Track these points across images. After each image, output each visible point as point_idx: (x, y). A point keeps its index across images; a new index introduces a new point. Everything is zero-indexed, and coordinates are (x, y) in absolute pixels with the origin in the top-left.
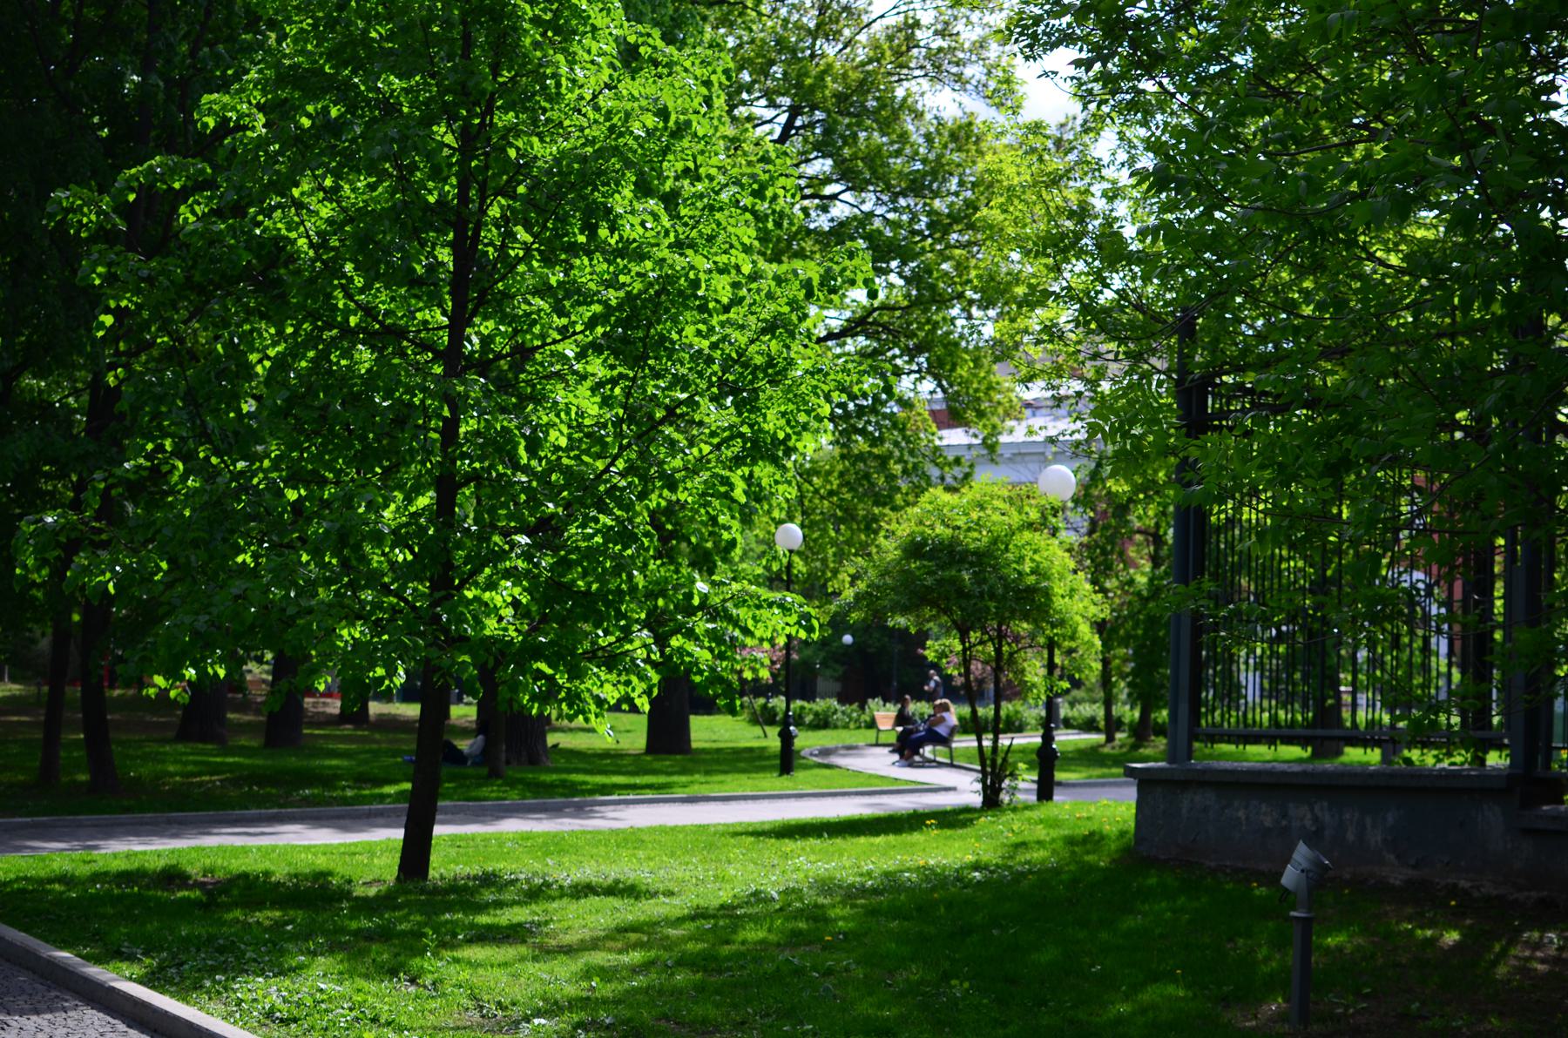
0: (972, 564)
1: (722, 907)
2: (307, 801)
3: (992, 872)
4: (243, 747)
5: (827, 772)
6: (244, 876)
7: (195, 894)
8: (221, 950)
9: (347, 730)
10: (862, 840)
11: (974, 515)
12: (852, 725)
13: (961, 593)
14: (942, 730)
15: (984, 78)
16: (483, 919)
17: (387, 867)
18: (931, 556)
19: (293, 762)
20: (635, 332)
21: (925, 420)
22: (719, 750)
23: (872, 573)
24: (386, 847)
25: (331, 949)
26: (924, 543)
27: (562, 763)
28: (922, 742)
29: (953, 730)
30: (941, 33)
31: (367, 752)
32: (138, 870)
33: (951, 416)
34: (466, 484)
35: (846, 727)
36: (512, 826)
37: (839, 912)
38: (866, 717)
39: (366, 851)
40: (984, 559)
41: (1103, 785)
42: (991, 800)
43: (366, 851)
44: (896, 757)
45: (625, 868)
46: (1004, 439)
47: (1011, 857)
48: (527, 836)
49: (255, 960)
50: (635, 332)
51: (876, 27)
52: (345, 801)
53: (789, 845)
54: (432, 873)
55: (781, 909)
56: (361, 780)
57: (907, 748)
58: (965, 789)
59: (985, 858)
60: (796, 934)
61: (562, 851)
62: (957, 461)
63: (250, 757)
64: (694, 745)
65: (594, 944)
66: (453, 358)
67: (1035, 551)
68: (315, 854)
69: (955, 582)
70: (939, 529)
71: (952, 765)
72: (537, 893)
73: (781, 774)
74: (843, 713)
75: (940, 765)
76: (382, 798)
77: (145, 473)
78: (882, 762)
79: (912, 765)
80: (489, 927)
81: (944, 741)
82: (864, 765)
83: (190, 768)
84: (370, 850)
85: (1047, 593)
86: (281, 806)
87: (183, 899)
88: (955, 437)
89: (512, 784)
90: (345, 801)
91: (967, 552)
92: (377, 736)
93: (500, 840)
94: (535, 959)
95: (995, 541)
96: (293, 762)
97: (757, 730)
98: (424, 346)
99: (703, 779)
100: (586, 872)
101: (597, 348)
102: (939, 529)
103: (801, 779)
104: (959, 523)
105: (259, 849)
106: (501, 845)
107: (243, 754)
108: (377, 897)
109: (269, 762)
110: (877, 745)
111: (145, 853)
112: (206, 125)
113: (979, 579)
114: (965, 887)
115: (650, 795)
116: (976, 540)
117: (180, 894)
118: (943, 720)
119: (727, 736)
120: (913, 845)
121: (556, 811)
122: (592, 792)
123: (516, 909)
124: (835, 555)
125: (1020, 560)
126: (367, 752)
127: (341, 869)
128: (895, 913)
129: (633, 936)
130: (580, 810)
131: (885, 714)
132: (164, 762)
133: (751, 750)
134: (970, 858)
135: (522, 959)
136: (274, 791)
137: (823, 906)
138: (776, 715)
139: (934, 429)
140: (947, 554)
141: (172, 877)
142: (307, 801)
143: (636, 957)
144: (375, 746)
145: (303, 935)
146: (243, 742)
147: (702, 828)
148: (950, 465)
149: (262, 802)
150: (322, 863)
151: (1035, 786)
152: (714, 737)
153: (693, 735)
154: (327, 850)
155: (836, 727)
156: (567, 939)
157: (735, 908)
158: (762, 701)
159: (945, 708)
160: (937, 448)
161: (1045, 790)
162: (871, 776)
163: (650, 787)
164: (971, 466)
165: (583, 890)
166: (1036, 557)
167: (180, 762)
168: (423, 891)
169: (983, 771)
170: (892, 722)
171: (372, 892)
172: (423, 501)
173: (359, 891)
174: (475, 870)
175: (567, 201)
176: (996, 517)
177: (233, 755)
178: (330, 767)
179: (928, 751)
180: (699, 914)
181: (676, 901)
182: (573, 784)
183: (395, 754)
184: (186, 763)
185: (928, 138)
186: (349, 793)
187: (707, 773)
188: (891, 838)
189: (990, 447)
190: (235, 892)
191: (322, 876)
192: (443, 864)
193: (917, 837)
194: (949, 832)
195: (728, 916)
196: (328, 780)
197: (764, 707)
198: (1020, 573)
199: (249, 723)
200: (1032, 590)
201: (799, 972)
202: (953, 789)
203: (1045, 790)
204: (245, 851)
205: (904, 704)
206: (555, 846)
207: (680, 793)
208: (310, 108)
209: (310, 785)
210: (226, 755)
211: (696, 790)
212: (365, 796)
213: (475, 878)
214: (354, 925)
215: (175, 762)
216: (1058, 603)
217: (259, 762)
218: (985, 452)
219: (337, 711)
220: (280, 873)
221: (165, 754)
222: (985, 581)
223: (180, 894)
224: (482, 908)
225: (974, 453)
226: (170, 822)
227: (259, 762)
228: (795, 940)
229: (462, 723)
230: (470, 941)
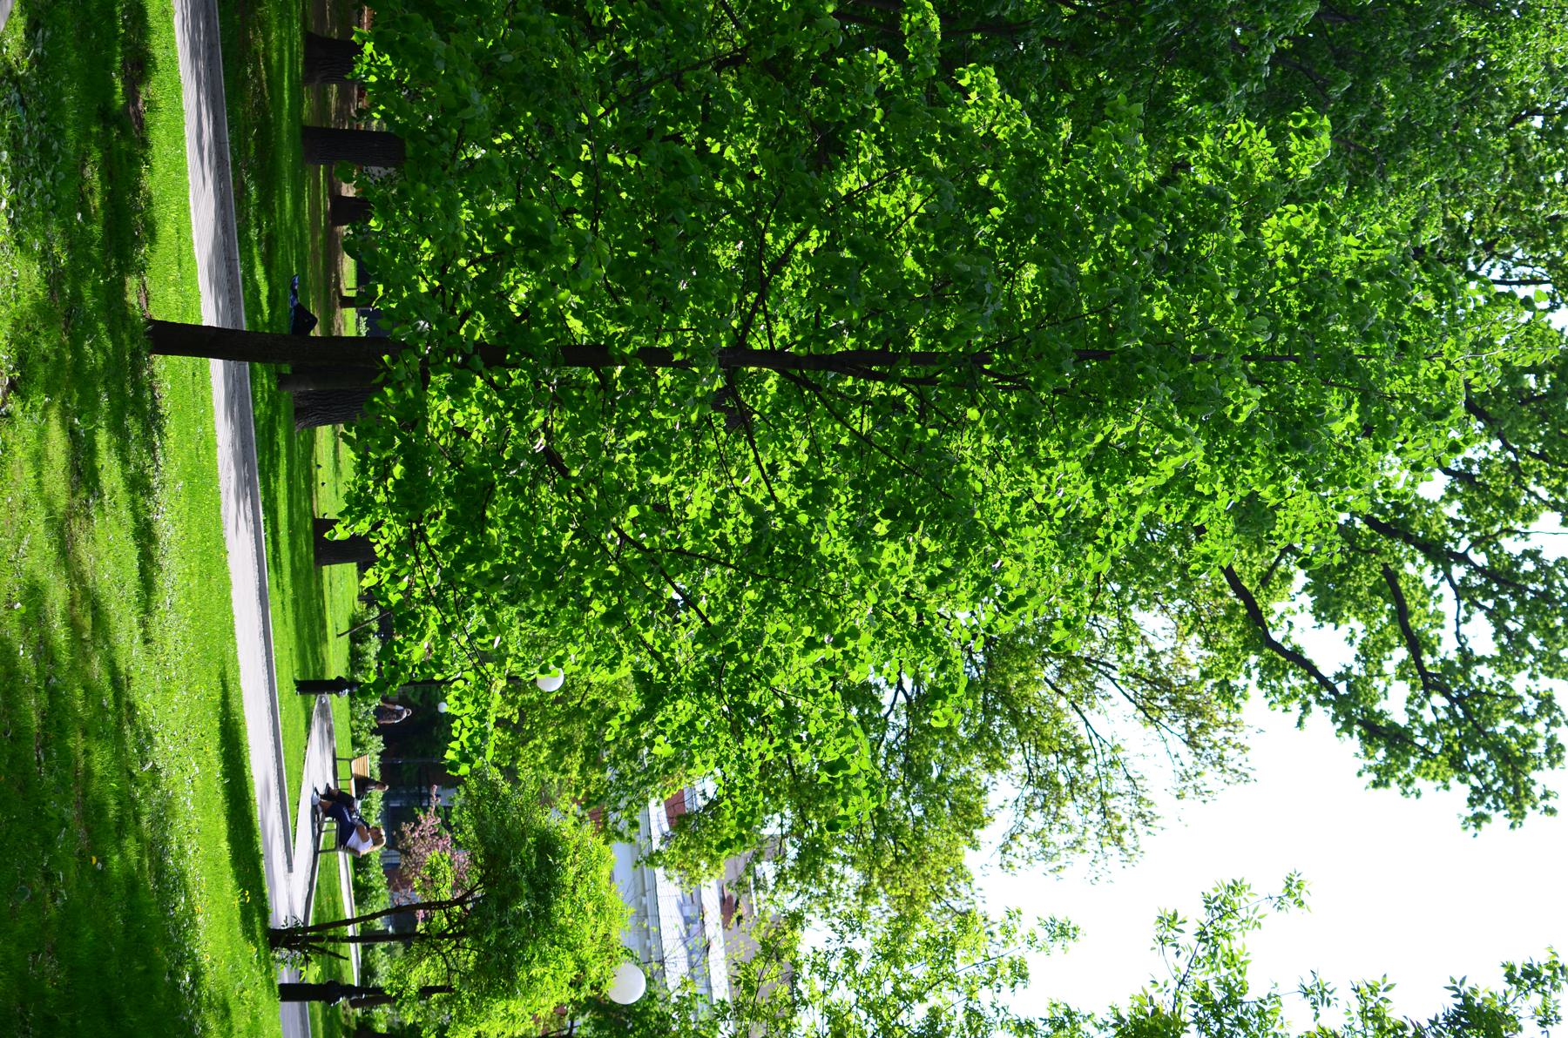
0: (535, 912)
1: (131, 707)
2: (241, 190)
3: (191, 993)
4: (301, 103)
5: (302, 727)
6: (145, 144)
7: (119, 99)
8: (44, 147)
9: (326, 204)
10: (223, 826)
11: (589, 906)
12: (354, 723)
13: (504, 904)
14: (354, 839)
15: (1030, 831)
16: (102, 438)
17: (166, 307)
18: (542, 861)
19: (287, 159)
20: (779, 559)
21: (675, 785)
22: (321, 593)
23: (519, 799)
24: (189, 302)
25: (54, 281)
26: (555, 854)
27: (300, 449)
28: (340, 818)
29: (354, 851)
30: (1072, 783)
31: (301, 233)
32: (148, 28)
33: (680, 818)
34: (598, 374)
35: (353, 717)
36: (223, 433)
37: (126, 856)
38: (364, 736)
39: (187, 273)
40: (543, 917)
41: (304, 1023)
42: (279, 939)
43: (187, 273)
44: (322, 791)
45: (174, 571)
46: (660, 872)
47: (210, 1005)
48: (210, 447)
49: (31, 191)
50: (779, 559)
51: (1075, 716)
52: (243, 231)
53: (213, 750)
54: (159, 359)
55: (132, 776)
56: (270, 242)
57: (333, 804)
58: (288, 899)
59: (208, 978)
60: (101, 808)
61: (192, 494)
62: (634, 825)
63: (291, 115)
64: (326, 568)
65: (76, 577)
66: (737, 357)
67: (553, 976)
68: (176, 221)
69: (516, 894)
70: (572, 870)
71: (316, 852)
72: (139, 485)
73: (296, 682)
74: (367, 713)
75: (316, 839)
76: (250, 270)
77: (594, 21)
78: (317, 775)
79: (314, 808)
80: (92, 451)
81: (342, 841)
82: (309, 759)
83: (275, 56)
84: (186, 279)
85: (509, 993)
86: (234, 164)
87: (112, 87)
88: (657, 816)
89: (273, 403)
90: (243, 231)
91: (549, 904)
92: (320, 237)
93: (204, 418)
94: (51, 520)
95: (562, 931)
96: (287, 159)
97: (344, 626)
98: (747, 323)
99: (288, 600)
100: (167, 526)
101: (761, 520)
102: (572, 870)
103: (293, 703)
104: (579, 890)
105: (182, 156)
106: (199, 421)
107: (293, 105)
108: (124, 305)
109: (285, 138)
110: (335, 759)
111: (171, 29)
112: (962, 76)
113: (519, 920)
114: (171, 974)
115: (267, 550)
116: (563, 911)
117: (118, 82)
118: (365, 840)
119: (337, 595)
120: (220, 888)
121: (242, 458)
122: (267, 490)
123: (117, 470)
124: (530, 700)
125: (544, 961)
126: (301, 233)
127: (159, 257)
128: (134, 914)
129: (87, 622)
130: (245, 484)
131: (368, 765)
132: (280, 26)
133: (323, 626)
134: (206, 960)
135: (49, 503)
136: (252, 152)
137: (138, 822)
138: (361, 642)
139: (667, 797)
140: (545, 885)
141: (140, 66)
142: (241, 190)
143: (60, 635)
144: (309, 238)
145: (76, 243)
146: (308, 104)
147: (229, 631)
148: (630, 816)
149: (239, 145)
150: (166, 230)
151: (311, 678)
152: (335, 583)
153: (337, 568)
154: (182, 232)
155: (352, 706)
156: (84, 551)
157: (131, 721)
158: (375, 626)
159: (376, 842)
160: (646, 801)
161: (290, 992)
162: (301, 774)
163: (275, 544)
164: (631, 840)
165: (145, 535)
166: (548, 978)
167: (282, 44)
168: (136, 355)
169: (307, 929)
170: (360, 773)
171: (132, 298)
172: (575, 325)
173: (132, 282)
174: (166, 406)
175: (923, 494)
176: (587, 929)
177: (291, 97)
178: (282, 203)
179: (330, 825)
180: (119, 683)
181: (138, 649)
182: (273, 466)
183: (301, 264)
184: (280, 51)
185: (964, 781)
186: (253, 233)
187: (295, 602)
188: (227, 857)
189: (652, 859)
190: (123, 145)
191: (151, 230)
192: (167, 369)
193: (230, 883)
194: (237, 918)
195: (118, 716)
196: (266, 205)
197: (370, 631)
198: (528, 962)
199: (328, 104)
200: (511, 976)
201: (48, 841)
202: (290, 869)
203: (290, 992)
204: (178, 141)
205: (380, 785)
206: (200, 479)
207: (270, 582)
208: (997, 185)
209: (260, 188)
210: (291, 89)
211: (275, 597)
212: (250, 251)
213: (156, 407)
214: (87, 293)
215: (281, 39)
216: (499, 1006)
217: (286, 123)
218: (646, 853)
219: (344, 193)
220: (153, 181)
221: (290, 25)
222: (518, 926)
223: (118, 82)
224: (118, 429)
225: (643, 843)
226: (210, 47)
227: (286, 123)
228: (93, 811)
229: (338, 321)
230: (72, 433)
